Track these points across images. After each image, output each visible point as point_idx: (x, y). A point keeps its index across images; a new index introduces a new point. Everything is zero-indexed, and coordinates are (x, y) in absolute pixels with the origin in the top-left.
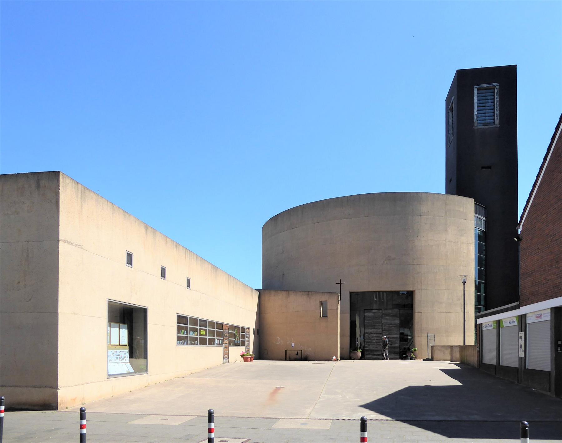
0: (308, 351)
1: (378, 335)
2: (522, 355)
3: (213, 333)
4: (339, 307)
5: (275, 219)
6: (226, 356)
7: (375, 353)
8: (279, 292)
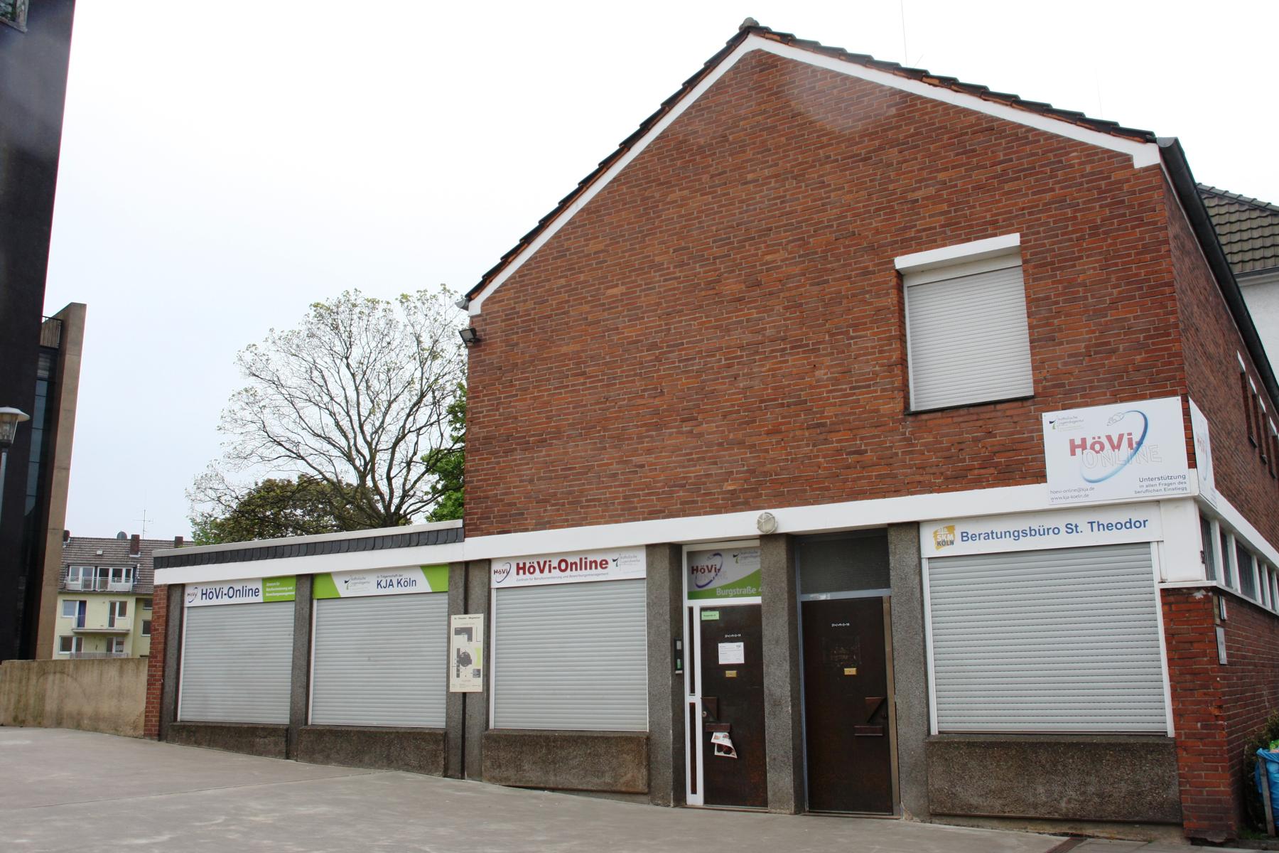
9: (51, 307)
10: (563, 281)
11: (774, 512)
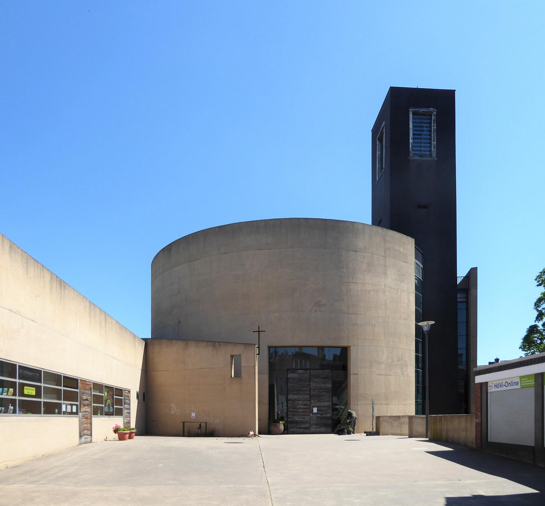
0: (215, 422)
1: (305, 402)
3: (57, 394)
4: (257, 363)
5: (168, 249)
6: (85, 431)
7: (302, 426)
8: (174, 342)
9: (462, 272)
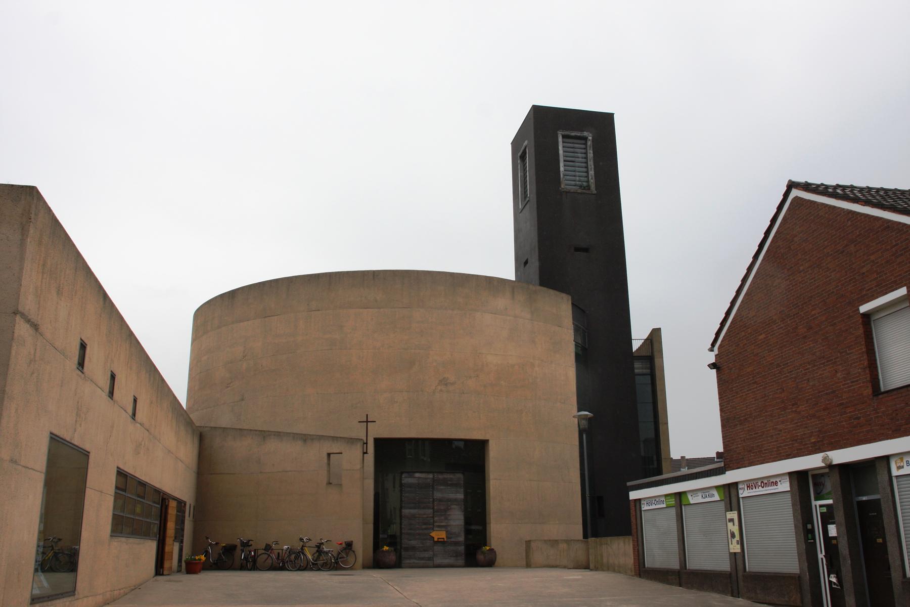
2: (735, 548)
9: (639, 335)
10: (743, 334)
11: (828, 453)
